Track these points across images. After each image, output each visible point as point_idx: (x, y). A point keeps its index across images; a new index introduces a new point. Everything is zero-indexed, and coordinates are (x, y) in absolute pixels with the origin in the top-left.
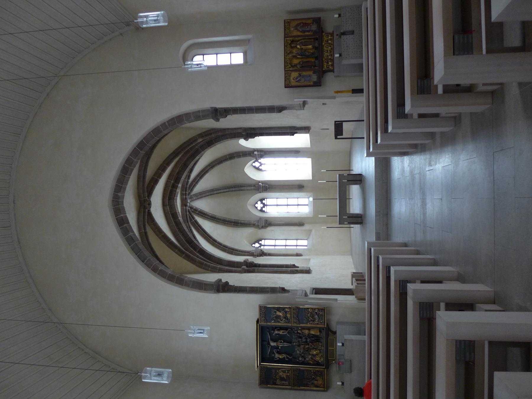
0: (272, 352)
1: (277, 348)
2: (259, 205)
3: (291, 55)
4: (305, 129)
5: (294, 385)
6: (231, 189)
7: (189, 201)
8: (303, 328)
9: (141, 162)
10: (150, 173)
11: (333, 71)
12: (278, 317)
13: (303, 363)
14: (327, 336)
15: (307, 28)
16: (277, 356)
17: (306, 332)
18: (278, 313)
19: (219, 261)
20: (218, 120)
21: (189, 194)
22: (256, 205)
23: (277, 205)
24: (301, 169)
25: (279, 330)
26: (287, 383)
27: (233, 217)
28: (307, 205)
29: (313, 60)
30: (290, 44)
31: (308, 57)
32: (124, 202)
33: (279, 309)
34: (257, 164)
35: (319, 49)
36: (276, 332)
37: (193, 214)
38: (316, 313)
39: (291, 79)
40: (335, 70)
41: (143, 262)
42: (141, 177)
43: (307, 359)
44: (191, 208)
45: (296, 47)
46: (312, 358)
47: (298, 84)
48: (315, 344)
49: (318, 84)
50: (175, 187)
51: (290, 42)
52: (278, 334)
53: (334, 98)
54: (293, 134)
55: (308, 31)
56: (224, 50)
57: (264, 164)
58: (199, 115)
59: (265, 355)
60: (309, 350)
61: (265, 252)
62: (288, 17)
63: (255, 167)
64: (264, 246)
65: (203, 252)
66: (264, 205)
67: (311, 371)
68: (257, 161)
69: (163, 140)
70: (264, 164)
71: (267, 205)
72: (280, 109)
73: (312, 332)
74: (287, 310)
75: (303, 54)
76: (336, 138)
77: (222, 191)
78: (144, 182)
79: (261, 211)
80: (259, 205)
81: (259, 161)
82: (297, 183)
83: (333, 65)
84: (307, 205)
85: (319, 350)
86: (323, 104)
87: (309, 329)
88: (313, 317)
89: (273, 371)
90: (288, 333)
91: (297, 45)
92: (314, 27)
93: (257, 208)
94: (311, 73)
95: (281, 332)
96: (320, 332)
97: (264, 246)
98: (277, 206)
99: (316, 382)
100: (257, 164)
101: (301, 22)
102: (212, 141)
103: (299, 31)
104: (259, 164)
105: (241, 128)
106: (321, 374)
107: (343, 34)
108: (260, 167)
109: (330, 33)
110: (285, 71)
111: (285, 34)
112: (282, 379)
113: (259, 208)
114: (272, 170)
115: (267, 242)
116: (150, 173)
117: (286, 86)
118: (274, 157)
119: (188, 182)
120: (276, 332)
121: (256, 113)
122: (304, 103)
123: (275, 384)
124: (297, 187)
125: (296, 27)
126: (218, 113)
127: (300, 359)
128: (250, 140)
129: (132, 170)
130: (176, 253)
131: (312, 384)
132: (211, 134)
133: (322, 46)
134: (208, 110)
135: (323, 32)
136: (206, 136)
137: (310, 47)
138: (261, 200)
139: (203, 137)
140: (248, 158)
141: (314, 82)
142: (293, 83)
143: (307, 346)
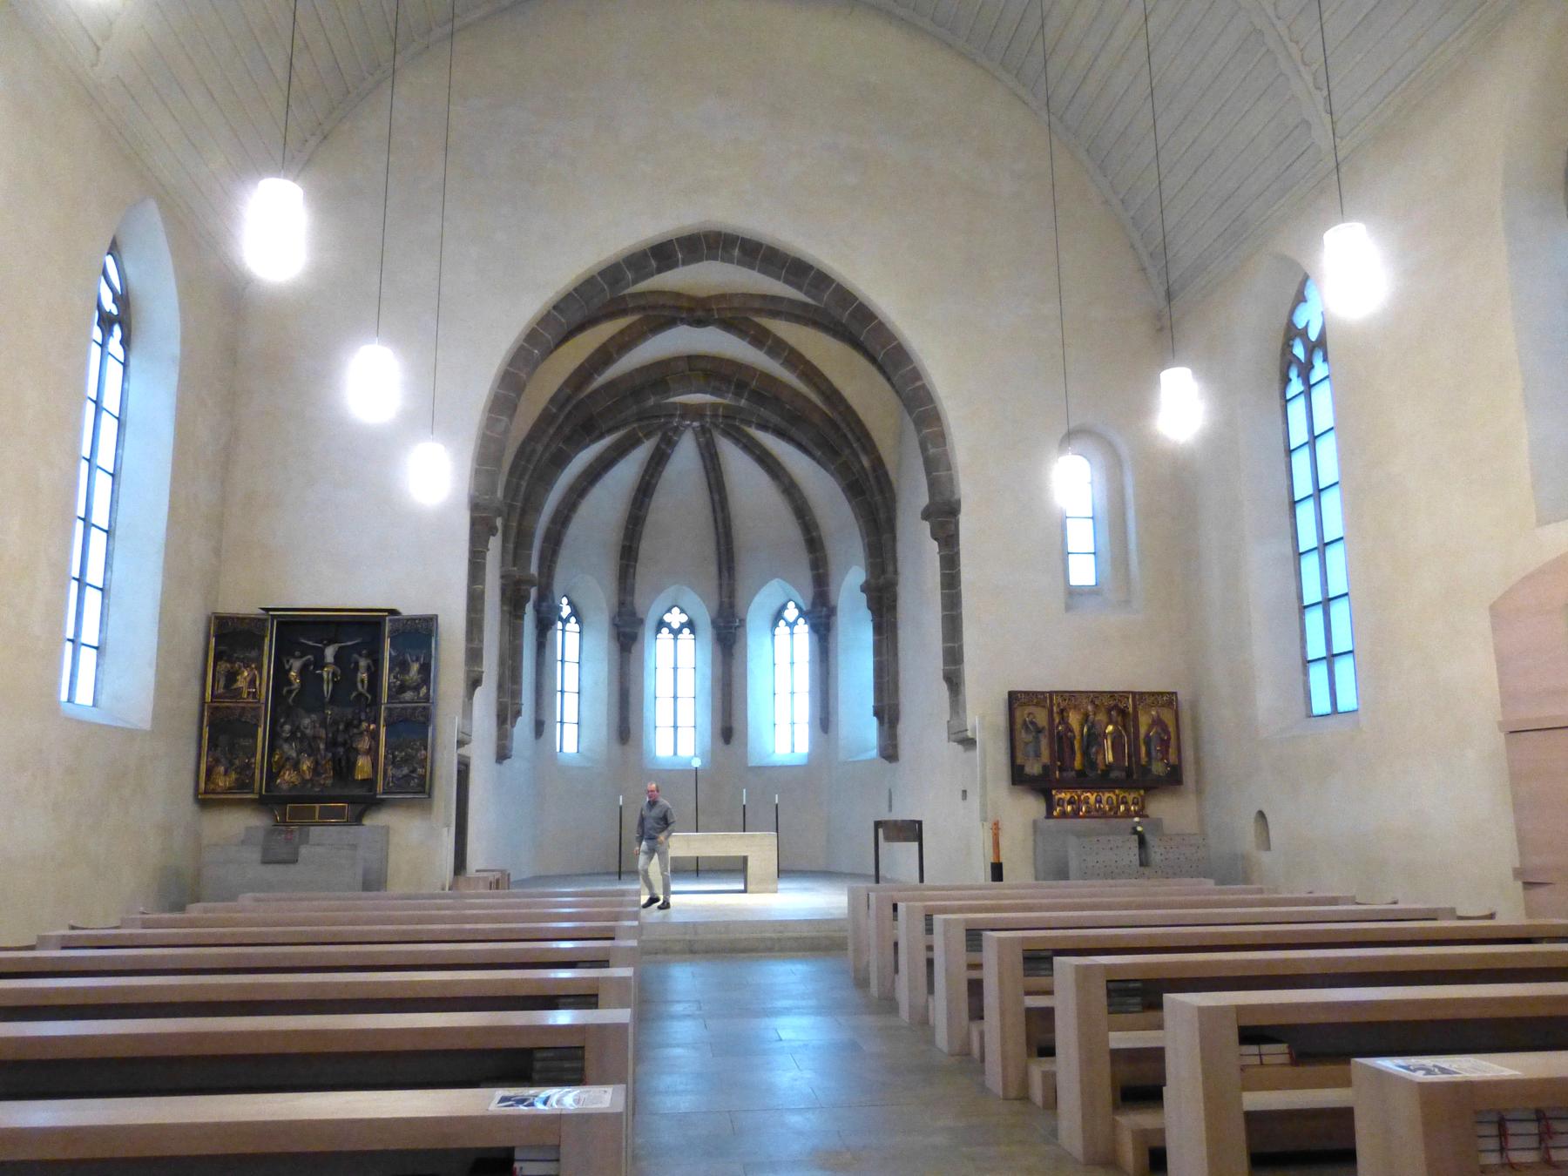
0: (305, 650)
1: (320, 663)
2: (675, 618)
3: (1090, 708)
4: (890, 751)
5: (214, 711)
7: (696, 424)
8: (375, 736)
9: (816, 309)
10: (782, 329)
11: (1049, 815)
13: (274, 735)
14: (352, 801)
15: (1156, 748)
16: (297, 664)
17: (364, 744)
18: (415, 667)
20: (927, 515)
21: (717, 426)
22: (676, 610)
23: (675, 669)
25: (368, 669)
26: (221, 691)
27: (645, 547)
29: (1078, 764)
30: (1120, 706)
31: (1086, 753)
32: (713, 263)
33: (425, 669)
34: (791, 613)
35: (1101, 780)
36: (363, 663)
38: (414, 771)
39: (1031, 709)
40: (1051, 821)
41: (555, 307)
42: (774, 306)
43: (286, 747)
44: (676, 430)
45: (1110, 722)
46: (288, 759)
47: (1018, 726)
48: (329, 766)
49: (1018, 777)
50: (740, 388)
51: (1122, 706)
52: (357, 668)
53: (984, 819)
55: (1148, 753)
56: (1104, 539)
57: (792, 634)
58: (937, 467)
59: (301, 630)
60: (312, 752)
61: (549, 633)
62: (1183, 697)
63: (784, 607)
64: (563, 630)
65: (560, 461)
66: (676, 633)
67: (254, 755)
68: (802, 614)
69: (873, 370)
70: (792, 634)
71: (676, 639)
72: (953, 681)
73: (363, 763)
74: (424, 690)
75: (1093, 738)
76: (878, 824)
77: (719, 516)
78: (759, 312)
79: (661, 624)
80: (675, 618)
81: (801, 621)
82: (736, 726)
83: (1064, 815)
87: (373, 752)
88: (407, 760)
89: (254, 654)
90: (360, 695)
91: (1115, 724)
92: (1158, 768)
93: (669, 611)
97: (563, 630)
98: (675, 665)
99: (222, 769)
100: (791, 613)
101: (1172, 729)
102: (862, 493)
103: (1150, 727)
104: (791, 620)
105: (896, 572)
106: (243, 785)
107: (1142, 842)
108: (782, 623)
109: (1143, 808)
110: (1051, 693)
111: (1142, 694)
112: (232, 677)
113: (667, 618)
114: (781, 658)
116: (782, 329)
117: (1013, 698)
118: (811, 662)
119: (749, 424)
121: (944, 617)
122: (968, 743)
123: (218, 657)
124: (728, 722)
125: (1158, 722)
126: (944, 517)
127: (287, 727)
128: (864, 596)
129: (799, 288)
130: (560, 390)
131: (217, 761)
132: (882, 492)
133: (1111, 788)
134: (953, 492)
135: (1147, 789)
136: (877, 477)
137: (1110, 757)
138: (690, 625)
139: (874, 470)
140: (810, 591)
141: (1022, 767)
142: (1021, 715)
143: (322, 746)
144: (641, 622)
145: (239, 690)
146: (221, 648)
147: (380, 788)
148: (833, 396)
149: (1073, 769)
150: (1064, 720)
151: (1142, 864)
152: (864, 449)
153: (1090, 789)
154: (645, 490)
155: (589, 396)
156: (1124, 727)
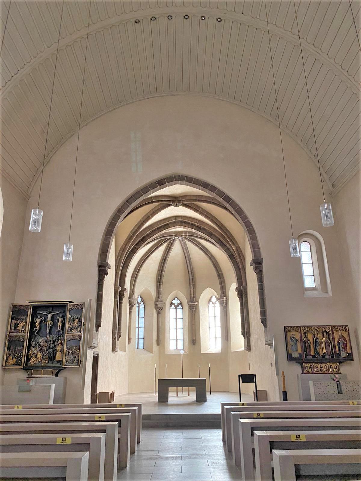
1: (46, 321)
2: (176, 302)
3: (315, 332)
4: (248, 347)
6: (191, 276)
7: (180, 238)
8: (62, 345)
12: (73, 320)
13: (30, 345)
15: (341, 346)
16: (38, 321)
18: (77, 320)
19: (126, 266)
20: (251, 265)
22: (176, 299)
24: (211, 342)
25: (62, 321)
27: (165, 278)
28: (177, 349)
29: (312, 353)
30: (327, 331)
31: (315, 349)
35: (323, 359)
36: (60, 320)
37: (168, 241)
38: (75, 357)
42: (200, 198)
43: (33, 349)
44: (174, 240)
45: (324, 337)
50: (192, 226)
54: (243, 334)
57: (215, 307)
60: (42, 350)
63: (212, 297)
65: (134, 251)
66: (176, 307)
67: (22, 352)
70: (215, 307)
71: (176, 309)
73: (58, 354)
74: (79, 329)
75: (317, 343)
79: (171, 304)
81: (217, 302)
84: (177, 349)
85: (41, 361)
86: (271, 363)
89: (24, 317)
92: (343, 354)
93: (174, 299)
94: (300, 351)
95: (60, 324)
96: (58, 362)
97: (139, 307)
100: (214, 299)
101: (347, 339)
106: (18, 363)
108: (211, 303)
109: (339, 370)
112: (16, 325)
113: (174, 302)
114: (210, 314)
115: (142, 310)
120: (60, 320)
125: (342, 337)
127: (34, 343)
132: (240, 257)
134: (260, 256)
135: (340, 363)
137: (325, 351)
139: (237, 250)
144: (165, 303)
145: (19, 330)
146: (14, 315)
147: (64, 363)
148: (221, 226)
149: (311, 355)
150: (306, 337)
151: (339, 393)
152: (234, 244)
153: (317, 363)
154: (164, 260)
155: (144, 230)
156: (329, 339)
